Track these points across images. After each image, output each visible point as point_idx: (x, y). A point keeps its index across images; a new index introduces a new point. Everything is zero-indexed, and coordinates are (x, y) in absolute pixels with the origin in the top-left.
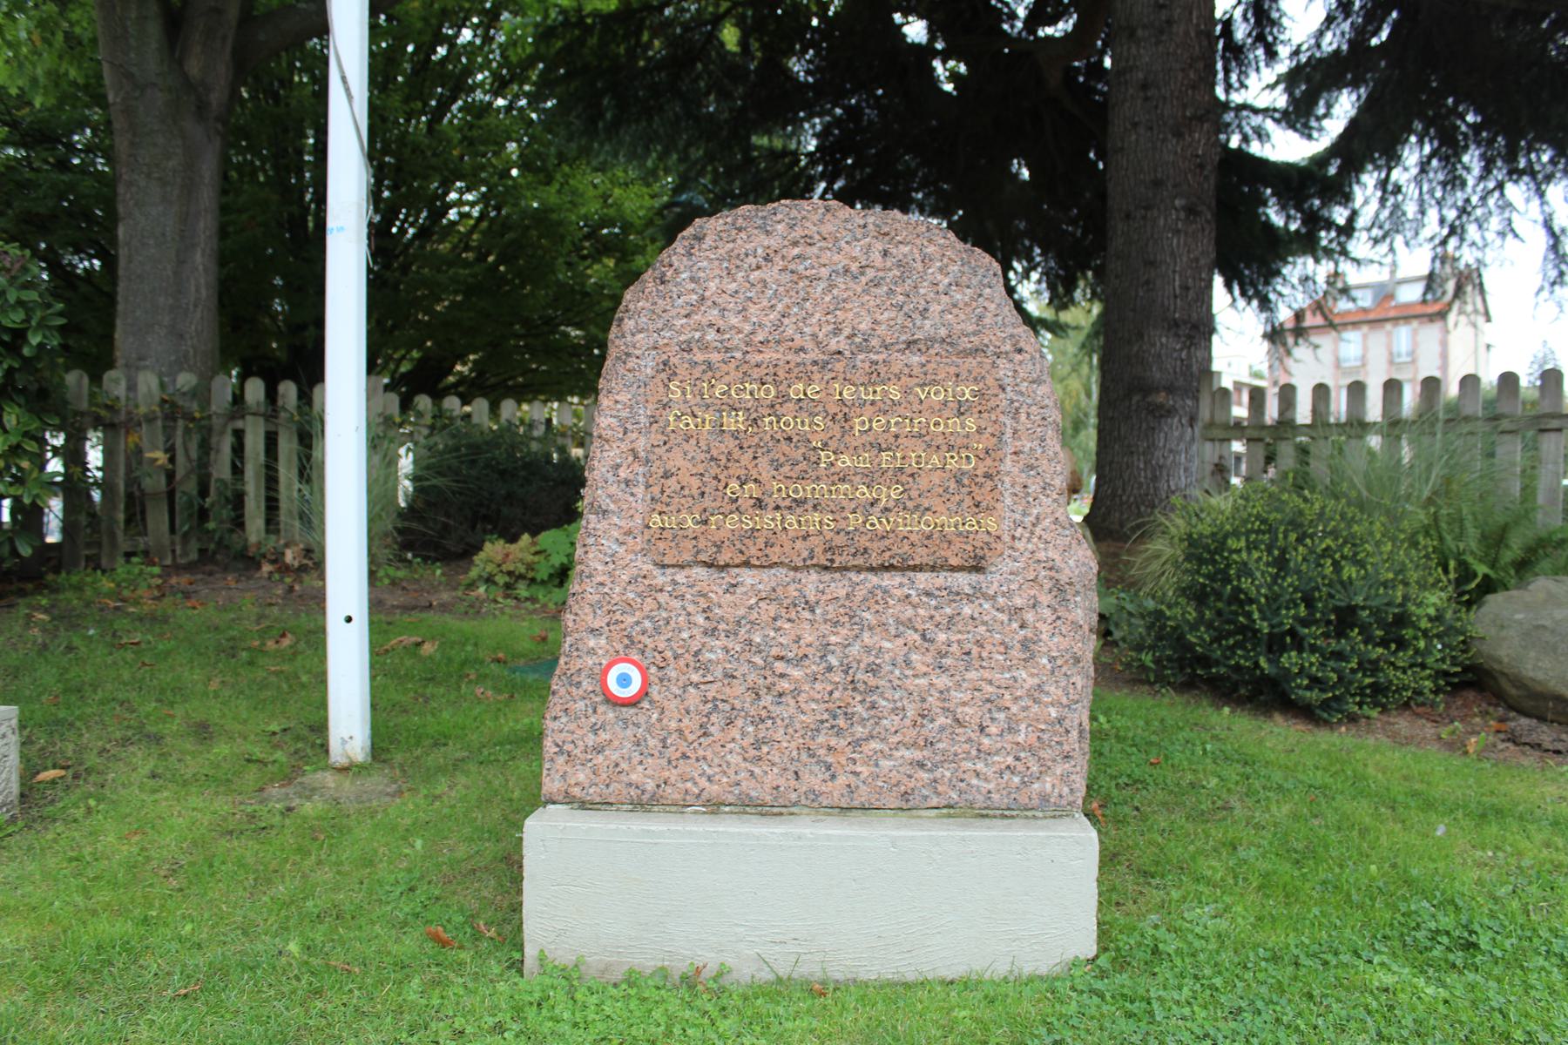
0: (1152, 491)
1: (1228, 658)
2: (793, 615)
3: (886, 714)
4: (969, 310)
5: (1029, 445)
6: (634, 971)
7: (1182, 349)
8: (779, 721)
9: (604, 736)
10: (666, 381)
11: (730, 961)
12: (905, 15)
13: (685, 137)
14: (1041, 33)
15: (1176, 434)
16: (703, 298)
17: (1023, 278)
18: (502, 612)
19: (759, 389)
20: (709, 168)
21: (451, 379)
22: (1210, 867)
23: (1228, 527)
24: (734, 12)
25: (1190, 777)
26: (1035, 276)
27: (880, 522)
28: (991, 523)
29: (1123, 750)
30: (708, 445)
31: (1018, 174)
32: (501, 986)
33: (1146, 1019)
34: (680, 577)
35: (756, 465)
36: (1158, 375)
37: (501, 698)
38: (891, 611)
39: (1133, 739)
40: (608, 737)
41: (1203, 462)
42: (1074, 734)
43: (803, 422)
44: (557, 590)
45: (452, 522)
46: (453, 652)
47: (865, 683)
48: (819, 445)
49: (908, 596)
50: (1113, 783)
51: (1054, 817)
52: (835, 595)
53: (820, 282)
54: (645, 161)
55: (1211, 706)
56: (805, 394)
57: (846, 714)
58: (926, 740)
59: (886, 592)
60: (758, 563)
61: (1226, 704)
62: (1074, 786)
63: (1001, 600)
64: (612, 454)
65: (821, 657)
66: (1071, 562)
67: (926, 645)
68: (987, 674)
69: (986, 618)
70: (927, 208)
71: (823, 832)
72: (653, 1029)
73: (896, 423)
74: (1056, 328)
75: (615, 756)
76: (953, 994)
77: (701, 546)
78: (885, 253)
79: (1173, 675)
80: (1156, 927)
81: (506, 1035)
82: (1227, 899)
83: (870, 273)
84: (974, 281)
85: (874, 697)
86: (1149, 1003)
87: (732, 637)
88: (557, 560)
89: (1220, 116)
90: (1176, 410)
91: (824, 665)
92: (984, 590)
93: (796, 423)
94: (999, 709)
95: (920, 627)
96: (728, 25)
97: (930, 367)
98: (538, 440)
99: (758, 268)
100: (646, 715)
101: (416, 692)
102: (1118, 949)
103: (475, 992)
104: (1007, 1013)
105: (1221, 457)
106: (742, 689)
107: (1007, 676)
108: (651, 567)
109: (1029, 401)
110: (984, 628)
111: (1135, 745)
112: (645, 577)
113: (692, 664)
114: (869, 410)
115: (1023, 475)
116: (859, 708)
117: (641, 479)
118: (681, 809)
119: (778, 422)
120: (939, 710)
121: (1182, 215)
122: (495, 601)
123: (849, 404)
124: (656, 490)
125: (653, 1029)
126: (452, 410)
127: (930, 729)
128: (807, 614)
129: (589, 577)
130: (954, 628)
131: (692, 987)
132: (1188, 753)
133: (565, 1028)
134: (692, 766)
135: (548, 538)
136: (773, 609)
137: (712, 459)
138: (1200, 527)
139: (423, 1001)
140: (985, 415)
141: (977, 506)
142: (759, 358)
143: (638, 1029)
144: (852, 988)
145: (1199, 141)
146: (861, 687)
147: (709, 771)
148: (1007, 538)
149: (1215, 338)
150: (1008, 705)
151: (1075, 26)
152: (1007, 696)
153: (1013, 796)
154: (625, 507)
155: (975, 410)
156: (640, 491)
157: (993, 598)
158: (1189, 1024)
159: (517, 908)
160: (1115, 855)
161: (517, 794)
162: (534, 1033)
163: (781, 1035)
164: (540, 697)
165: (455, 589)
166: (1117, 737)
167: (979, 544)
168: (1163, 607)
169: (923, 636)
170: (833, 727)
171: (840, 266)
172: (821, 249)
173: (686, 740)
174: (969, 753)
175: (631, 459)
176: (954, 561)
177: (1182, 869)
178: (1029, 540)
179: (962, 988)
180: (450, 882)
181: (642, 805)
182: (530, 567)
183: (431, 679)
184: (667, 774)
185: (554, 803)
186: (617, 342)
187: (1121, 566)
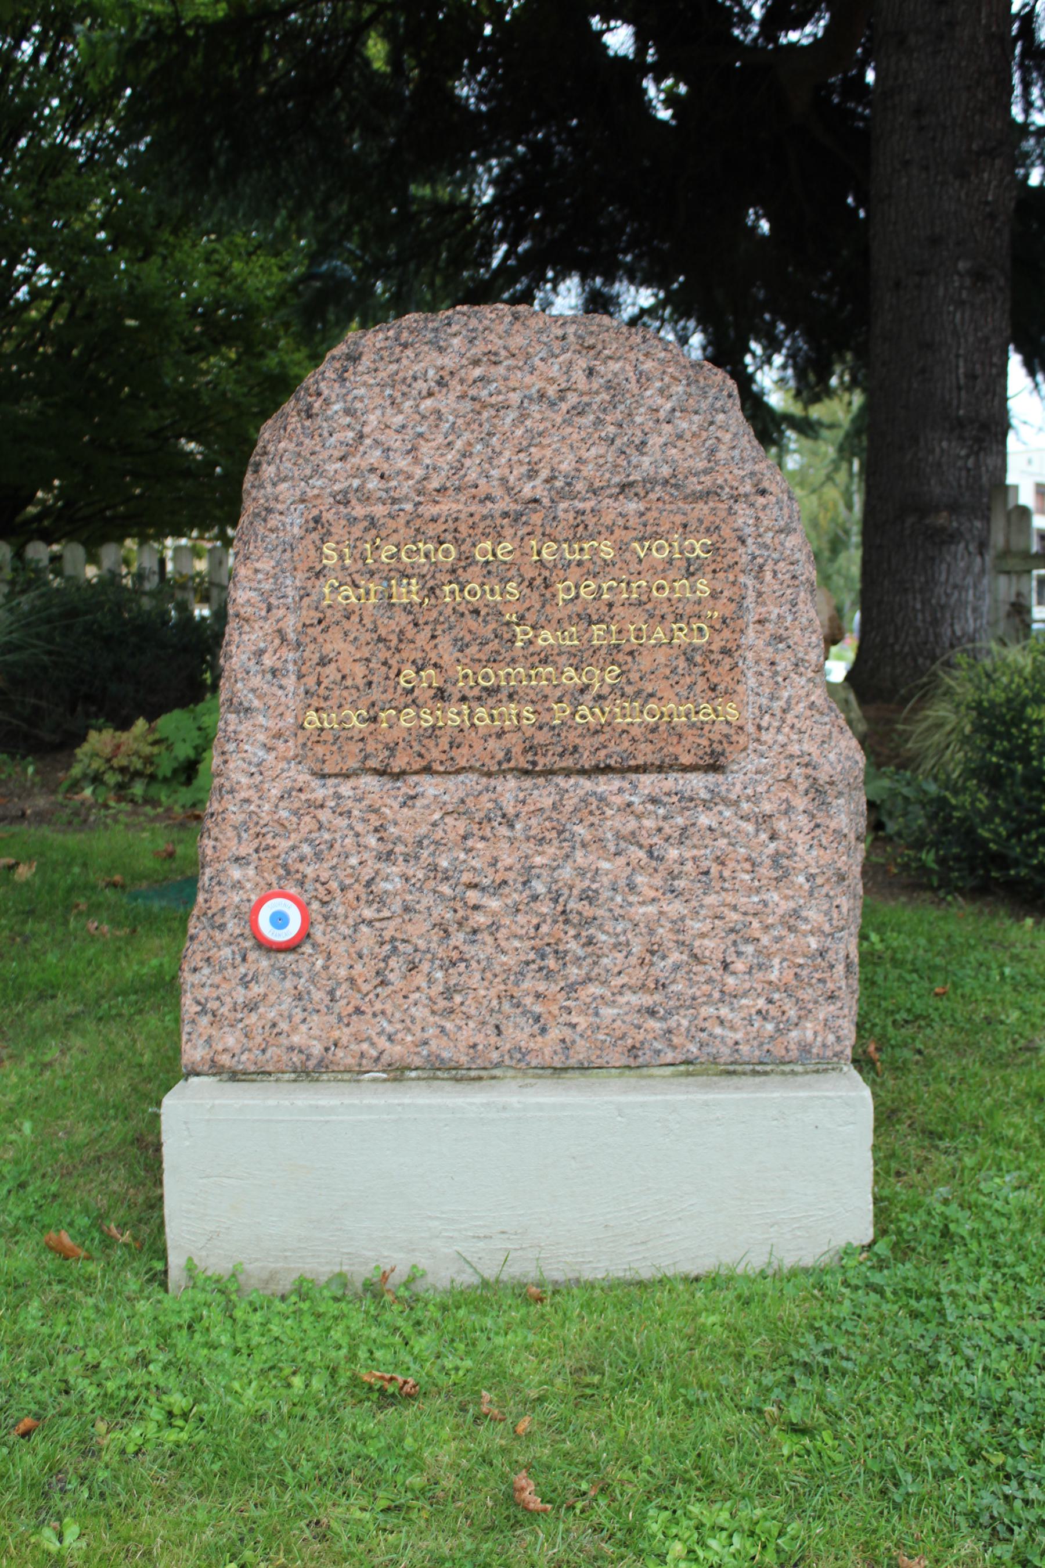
0: (932, 638)
1: (1031, 857)
2: (488, 833)
3: (606, 951)
4: (696, 442)
5: (776, 611)
6: (305, 1279)
7: (968, 456)
8: (474, 964)
9: (256, 989)
10: (318, 542)
11: (424, 1262)
12: (605, 19)
13: (322, 187)
14: (783, 41)
15: (962, 564)
16: (361, 436)
17: (763, 363)
18: (116, 821)
19: (436, 550)
20: (356, 229)
21: (32, 510)
22: (1010, 1125)
23: (1026, 692)
24: (381, 17)
25: (984, 1010)
26: (778, 360)
27: (593, 714)
28: (731, 711)
29: (900, 978)
30: (375, 622)
31: (755, 227)
32: (142, 1306)
33: (936, 1319)
34: (345, 789)
35: (436, 646)
36: (937, 490)
37: (120, 933)
38: (609, 823)
39: (913, 963)
40: (262, 990)
41: (996, 601)
42: (840, 968)
43: (492, 591)
44: (184, 789)
45: (44, 704)
46: (57, 876)
47: (579, 913)
48: (514, 619)
49: (629, 805)
50: (889, 1021)
51: (817, 1072)
52: (539, 805)
53: (509, 411)
54: (273, 220)
55: (1010, 917)
56: (494, 555)
57: (556, 952)
58: (657, 982)
59: (602, 799)
60: (442, 769)
61: (1028, 914)
62: (841, 1033)
63: (745, 806)
64: (253, 637)
65: (524, 883)
66: (832, 757)
67: (654, 863)
68: (730, 898)
69: (727, 829)
70: (639, 275)
71: (533, 1100)
72: (333, 1354)
73: (610, 588)
74: (807, 428)
75: (272, 1014)
76: (699, 1294)
77: (370, 749)
78: (591, 372)
79: (962, 878)
80: (946, 1202)
81: (151, 1367)
82: (1033, 1165)
83: (572, 398)
84: (704, 405)
85: (592, 931)
86: (939, 1300)
87: (412, 862)
88: (184, 751)
89: (1016, 145)
90: (961, 534)
91: (528, 892)
92: (724, 793)
93: (484, 592)
94: (747, 941)
95: (646, 842)
96: (373, 34)
97: (650, 516)
98: (151, 594)
99: (430, 394)
100: (310, 961)
101: (11, 930)
102: (900, 1232)
103: (110, 1314)
104: (766, 1317)
105: (1019, 594)
106: (427, 925)
107: (756, 899)
108: (308, 777)
109: (775, 556)
110: (725, 841)
111: (916, 971)
112: (300, 790)
113: (364, 897)
114: (575, 573)
115: (770, 649)
116: (573, 945)
117: (291, 667)
118: (355, 1076)
119: (462, 591)
120: (671, 945)
121: (968, 282)
122: (106, 806)
123: (550, 565)
124: (311, 681)
125: (333, 1354)
126: (39, 561)
127: (661, 968)
128: (504, 831)
129: (231, 791)
130: (688, 842)
131: (377, 1296)
132: (982, 978)
133: (224, 1356)
134: (367, 1022)
135: (171, 722)
136: (462, 826)
137: (380, 639)
138: (992, 692)
139: (45, 1330)
140: (721, 575)
141: (713, 690)
142: (435, 510)
143: (314, 1354)
144: (575, 1291)
145: (990, 182)
146: (575, 918)
147: (390, 1029)
148: (750, 728)
149: (1011, 439)
150: (757, 935)
151: (827, 28)
152: (756, 924)
153: (766, 1047)
154: (272, 703)
155: (709, 569)
156: (290, 682)
157: (736, 803)
158: (988, 1325)
159: (156, 1204)
160: (894, 1111)
161: (147, 1058)
162: (187, 1363)
163: (490, 1355)
164: (170, 930)
165: (54, 792)
166: (893, 960)
167: (716, 737)
168: (948, 794)
169: (650, 854)
170: (541, 969)
171: (534, 390)
172: (509, 369)
173: (359, 991)
174: (710, 995)
175: (277, 642)
176: (686, 759)
177: (977, 1127)
178: (779, 730)
179: (710, 1286)
180: (70, 1174)
181: (308, 1074)
182: (148, 760)
183: (31, 912)
184: (337, 1034)
185: (198, 1074)
186: (254, 493)
187: (895, 736)
